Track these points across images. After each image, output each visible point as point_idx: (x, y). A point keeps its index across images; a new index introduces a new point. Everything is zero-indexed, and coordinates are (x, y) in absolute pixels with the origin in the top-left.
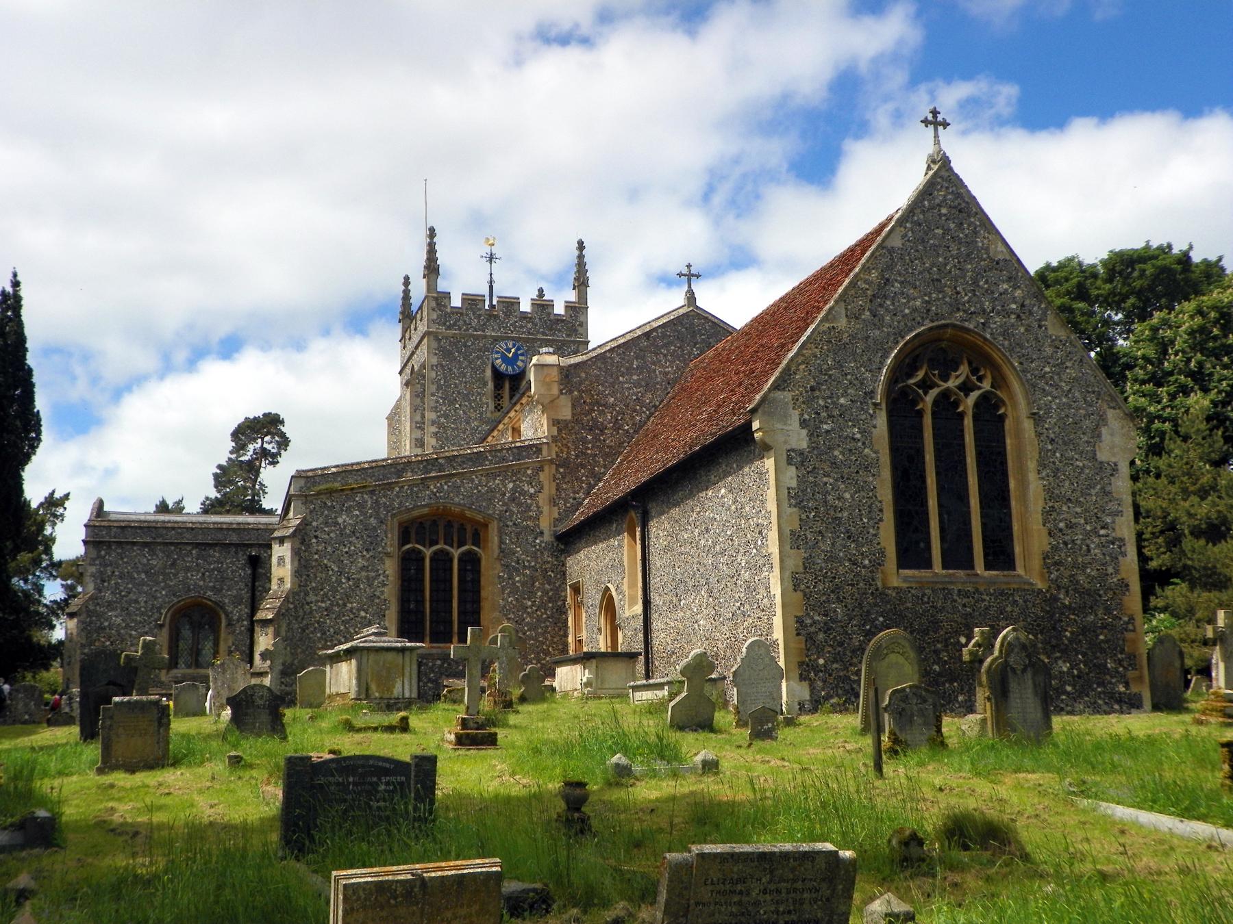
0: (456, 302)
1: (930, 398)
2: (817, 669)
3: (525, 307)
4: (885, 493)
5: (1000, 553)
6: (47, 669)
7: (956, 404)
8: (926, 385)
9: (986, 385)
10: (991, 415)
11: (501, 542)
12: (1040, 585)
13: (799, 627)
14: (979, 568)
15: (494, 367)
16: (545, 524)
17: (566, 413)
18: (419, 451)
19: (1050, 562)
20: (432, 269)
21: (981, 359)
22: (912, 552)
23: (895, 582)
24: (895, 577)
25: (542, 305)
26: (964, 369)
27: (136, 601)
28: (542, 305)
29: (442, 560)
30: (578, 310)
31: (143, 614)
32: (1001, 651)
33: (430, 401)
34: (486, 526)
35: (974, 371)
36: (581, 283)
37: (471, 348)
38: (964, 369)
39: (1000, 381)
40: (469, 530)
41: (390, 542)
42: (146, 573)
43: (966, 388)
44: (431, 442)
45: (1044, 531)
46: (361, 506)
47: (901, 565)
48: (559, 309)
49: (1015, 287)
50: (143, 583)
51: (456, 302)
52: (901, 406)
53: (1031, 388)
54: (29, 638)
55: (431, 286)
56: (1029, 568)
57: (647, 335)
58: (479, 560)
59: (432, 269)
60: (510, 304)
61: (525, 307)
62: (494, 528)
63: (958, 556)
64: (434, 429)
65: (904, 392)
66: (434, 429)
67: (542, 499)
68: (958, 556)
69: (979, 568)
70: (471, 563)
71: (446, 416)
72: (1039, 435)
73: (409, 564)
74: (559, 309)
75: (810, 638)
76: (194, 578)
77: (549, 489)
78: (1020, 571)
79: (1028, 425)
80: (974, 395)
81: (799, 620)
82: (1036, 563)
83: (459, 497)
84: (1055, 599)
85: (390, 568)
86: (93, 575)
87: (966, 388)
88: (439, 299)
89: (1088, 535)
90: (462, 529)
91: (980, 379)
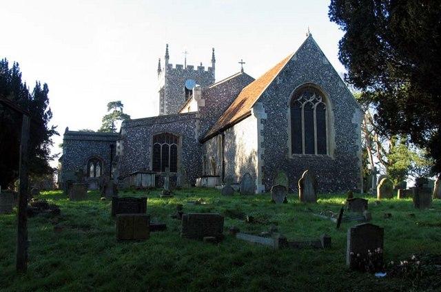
0: (174, 67)
1: (303, 105)
2: (267, 181)
3: (196, 69)
4: (289, 132)
5: (322, 149)
6: (30, 217)
7: (312, 106)
8: (303, 100)
9: (320, 101)
10: (321, 108)
11: (183, 142)
12: (333, 159)
13: (263, 169)
14: (316, 154)
15: (186, 88)
16: (196, 137)
17: (203, 105)
18: (162, 113)
19: (336, 152)
20: (167, 57)
21: (318, 93)
22: (297, 149)
23: (291, 157)
24: (290, 156)
25: (201, 68)
26: (314, 96)
28: (201, 68)
29: (165, 148)
30: (212, 69)
32: (101, 174)
33: (166, 98)
34: (179, 137)
35: (317, 96)
36: (214, 61)
37: (179, 80)
38: (314, 96)
39: (324, 100)
40: (172, 138)
41: (151, 142)
43: (315, 101)
44: (166, 110)
45: (335, 143)
46: (142, 131)
47: (293, 152)
48: (206, 69)
49: (330, 72)
51: (174, 67)
52: (295, 105)
53: (334, 102)
54: (47, 164)
55: (167, 62)
56: (330, 154)
57: (229, 81)
58: (176, 148)
59: (167, 57)
60: (192, 67)
61: (196, 69)
62: (181, 137)
63: (310, 150)
65: (297, 102)
67: (196, 130)
68: (310, 150)
69: (316, 154)
70: (174, 148)
71: (171, 103)
72: (335, 115)
73: (156, 148)
74: (206, 69)
75: (265, 173)
76: (95, 151)
77: (198, 127)
78: (328, 154)
79: (332, 112)
80: (317, 104)
81: (262, 167)
82: (332, 152)
83: (171, 128)
84: (337, 163)
85: (150, 149)
87: (315, 101)
88: (169, 66)
89: (347, 144)
90: (172, 138)
91: (319, 99)
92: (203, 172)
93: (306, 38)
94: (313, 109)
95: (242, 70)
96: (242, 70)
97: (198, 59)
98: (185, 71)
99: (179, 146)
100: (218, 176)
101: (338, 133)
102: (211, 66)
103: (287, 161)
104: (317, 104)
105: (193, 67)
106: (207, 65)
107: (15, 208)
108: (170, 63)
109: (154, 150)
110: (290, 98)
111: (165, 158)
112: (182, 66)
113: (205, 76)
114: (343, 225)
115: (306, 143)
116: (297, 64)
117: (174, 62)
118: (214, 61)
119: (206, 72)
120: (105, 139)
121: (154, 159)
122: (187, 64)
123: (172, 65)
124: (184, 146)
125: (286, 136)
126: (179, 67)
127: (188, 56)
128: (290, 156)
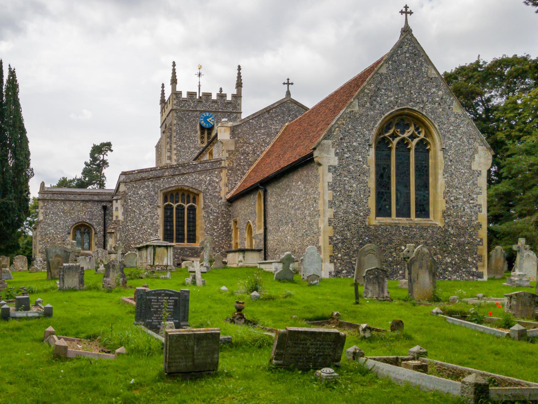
0: (184, 95)
3: (214, 97)
5: (423, 210)
8: (394, 136)
9: (422, 136)
19: (445, 214)
20: (174, 81)
21: (419, 122)
22: (382, 210)
24: (374, 220)
25: (222, 96)
27: (59, 224)
28: (222, 96)
29: (180, 209)
30: (237, 97)
31: (62, 229)
34: (198, 195)
35: (417, 129)
36: (239, 85)
39: (428, 133)
41: (160, 201)
42: (63, 212)
43: (413, 137)
45: (444, 201)
48: (229, 98)
49: (439, 90)
50: (61, 217)
51: (184, 95)
52: (382, 145)
56: (436, 219)
59: (174, 81)
61: (214, 97)
62: (201, 196)
64: (175, 152)
66: (175, 152)
67: (222, 184)
70: (192, 210)
71: (180, 146)
73: (168, 209)
74: (229, 98)
75: (335, 246)
82: (440, 215)
84: (447, 231)
85: (160, 212)
86: (42, 213)
87: (413, 137)
88: (176, 94)
90: (188, 196)
91: (419, 133)
92: (233, 243)
93: (396, 38)
94: (409, 150)
95: (288, 93)
96: (288, 93)
97: (215, 81)
98: (200, 101)
99: (200, 206)
100: (259, 251)
101: (448, 185)
102: (235, 92)
103: (368, 228)
104: (397, 139)
105: (210, 95)
106: (230, 92)
107: (87, 179)
108: (178, 89)
109: (165, 212)
110: (374, 132)
111: (180, 225)
112: (195, 94)
113: (228, 106)
114: (360, 300)
115: (397, 200)
116: (386, 78)
117: (185, 87)
118: (239, 85)
119: (229, 103)
120: (96, 198)
121: (165, 226)
122: (203, 90)
123: (180, 93)
124: (206, 207)
125: (366, 192)
126: (191, 95)
127: (202, 78)
128: (374, 220)
